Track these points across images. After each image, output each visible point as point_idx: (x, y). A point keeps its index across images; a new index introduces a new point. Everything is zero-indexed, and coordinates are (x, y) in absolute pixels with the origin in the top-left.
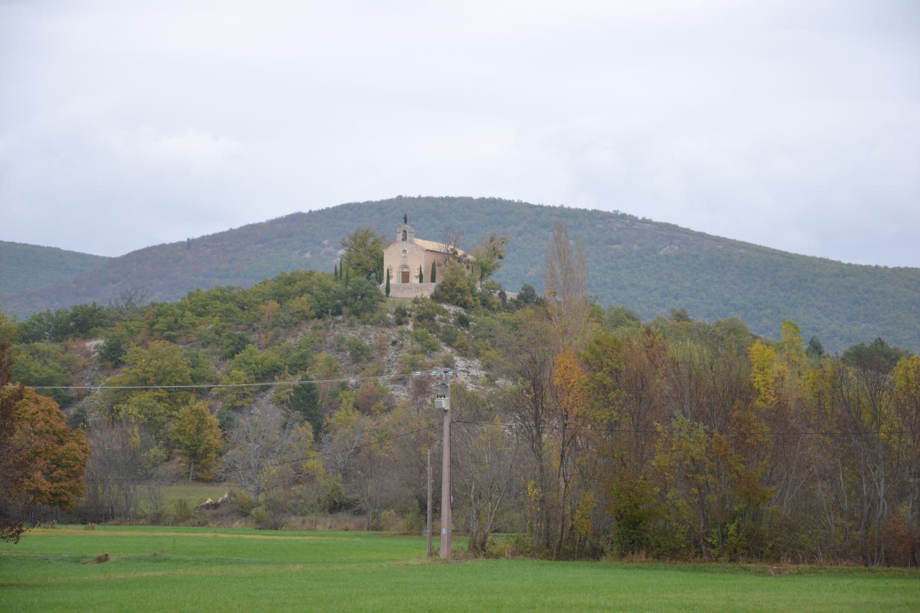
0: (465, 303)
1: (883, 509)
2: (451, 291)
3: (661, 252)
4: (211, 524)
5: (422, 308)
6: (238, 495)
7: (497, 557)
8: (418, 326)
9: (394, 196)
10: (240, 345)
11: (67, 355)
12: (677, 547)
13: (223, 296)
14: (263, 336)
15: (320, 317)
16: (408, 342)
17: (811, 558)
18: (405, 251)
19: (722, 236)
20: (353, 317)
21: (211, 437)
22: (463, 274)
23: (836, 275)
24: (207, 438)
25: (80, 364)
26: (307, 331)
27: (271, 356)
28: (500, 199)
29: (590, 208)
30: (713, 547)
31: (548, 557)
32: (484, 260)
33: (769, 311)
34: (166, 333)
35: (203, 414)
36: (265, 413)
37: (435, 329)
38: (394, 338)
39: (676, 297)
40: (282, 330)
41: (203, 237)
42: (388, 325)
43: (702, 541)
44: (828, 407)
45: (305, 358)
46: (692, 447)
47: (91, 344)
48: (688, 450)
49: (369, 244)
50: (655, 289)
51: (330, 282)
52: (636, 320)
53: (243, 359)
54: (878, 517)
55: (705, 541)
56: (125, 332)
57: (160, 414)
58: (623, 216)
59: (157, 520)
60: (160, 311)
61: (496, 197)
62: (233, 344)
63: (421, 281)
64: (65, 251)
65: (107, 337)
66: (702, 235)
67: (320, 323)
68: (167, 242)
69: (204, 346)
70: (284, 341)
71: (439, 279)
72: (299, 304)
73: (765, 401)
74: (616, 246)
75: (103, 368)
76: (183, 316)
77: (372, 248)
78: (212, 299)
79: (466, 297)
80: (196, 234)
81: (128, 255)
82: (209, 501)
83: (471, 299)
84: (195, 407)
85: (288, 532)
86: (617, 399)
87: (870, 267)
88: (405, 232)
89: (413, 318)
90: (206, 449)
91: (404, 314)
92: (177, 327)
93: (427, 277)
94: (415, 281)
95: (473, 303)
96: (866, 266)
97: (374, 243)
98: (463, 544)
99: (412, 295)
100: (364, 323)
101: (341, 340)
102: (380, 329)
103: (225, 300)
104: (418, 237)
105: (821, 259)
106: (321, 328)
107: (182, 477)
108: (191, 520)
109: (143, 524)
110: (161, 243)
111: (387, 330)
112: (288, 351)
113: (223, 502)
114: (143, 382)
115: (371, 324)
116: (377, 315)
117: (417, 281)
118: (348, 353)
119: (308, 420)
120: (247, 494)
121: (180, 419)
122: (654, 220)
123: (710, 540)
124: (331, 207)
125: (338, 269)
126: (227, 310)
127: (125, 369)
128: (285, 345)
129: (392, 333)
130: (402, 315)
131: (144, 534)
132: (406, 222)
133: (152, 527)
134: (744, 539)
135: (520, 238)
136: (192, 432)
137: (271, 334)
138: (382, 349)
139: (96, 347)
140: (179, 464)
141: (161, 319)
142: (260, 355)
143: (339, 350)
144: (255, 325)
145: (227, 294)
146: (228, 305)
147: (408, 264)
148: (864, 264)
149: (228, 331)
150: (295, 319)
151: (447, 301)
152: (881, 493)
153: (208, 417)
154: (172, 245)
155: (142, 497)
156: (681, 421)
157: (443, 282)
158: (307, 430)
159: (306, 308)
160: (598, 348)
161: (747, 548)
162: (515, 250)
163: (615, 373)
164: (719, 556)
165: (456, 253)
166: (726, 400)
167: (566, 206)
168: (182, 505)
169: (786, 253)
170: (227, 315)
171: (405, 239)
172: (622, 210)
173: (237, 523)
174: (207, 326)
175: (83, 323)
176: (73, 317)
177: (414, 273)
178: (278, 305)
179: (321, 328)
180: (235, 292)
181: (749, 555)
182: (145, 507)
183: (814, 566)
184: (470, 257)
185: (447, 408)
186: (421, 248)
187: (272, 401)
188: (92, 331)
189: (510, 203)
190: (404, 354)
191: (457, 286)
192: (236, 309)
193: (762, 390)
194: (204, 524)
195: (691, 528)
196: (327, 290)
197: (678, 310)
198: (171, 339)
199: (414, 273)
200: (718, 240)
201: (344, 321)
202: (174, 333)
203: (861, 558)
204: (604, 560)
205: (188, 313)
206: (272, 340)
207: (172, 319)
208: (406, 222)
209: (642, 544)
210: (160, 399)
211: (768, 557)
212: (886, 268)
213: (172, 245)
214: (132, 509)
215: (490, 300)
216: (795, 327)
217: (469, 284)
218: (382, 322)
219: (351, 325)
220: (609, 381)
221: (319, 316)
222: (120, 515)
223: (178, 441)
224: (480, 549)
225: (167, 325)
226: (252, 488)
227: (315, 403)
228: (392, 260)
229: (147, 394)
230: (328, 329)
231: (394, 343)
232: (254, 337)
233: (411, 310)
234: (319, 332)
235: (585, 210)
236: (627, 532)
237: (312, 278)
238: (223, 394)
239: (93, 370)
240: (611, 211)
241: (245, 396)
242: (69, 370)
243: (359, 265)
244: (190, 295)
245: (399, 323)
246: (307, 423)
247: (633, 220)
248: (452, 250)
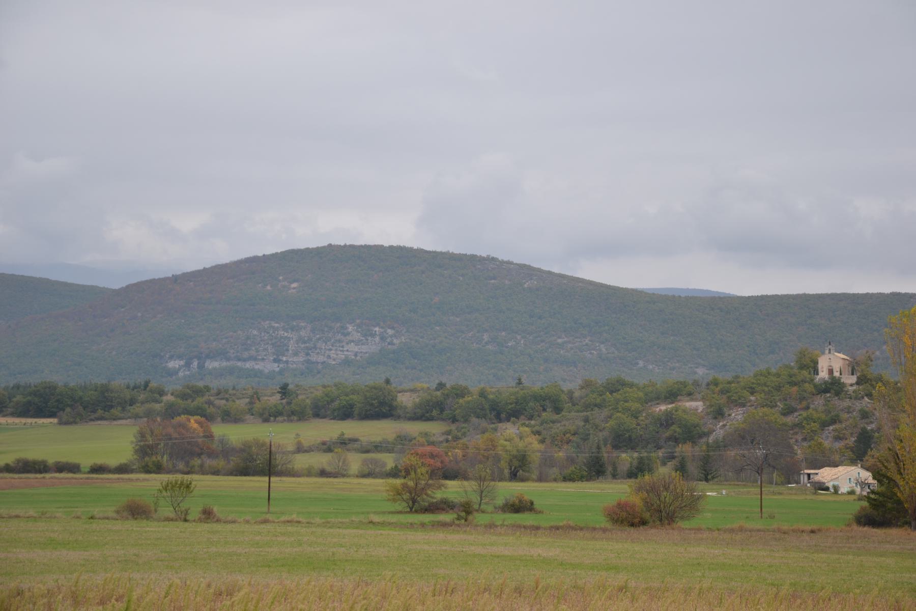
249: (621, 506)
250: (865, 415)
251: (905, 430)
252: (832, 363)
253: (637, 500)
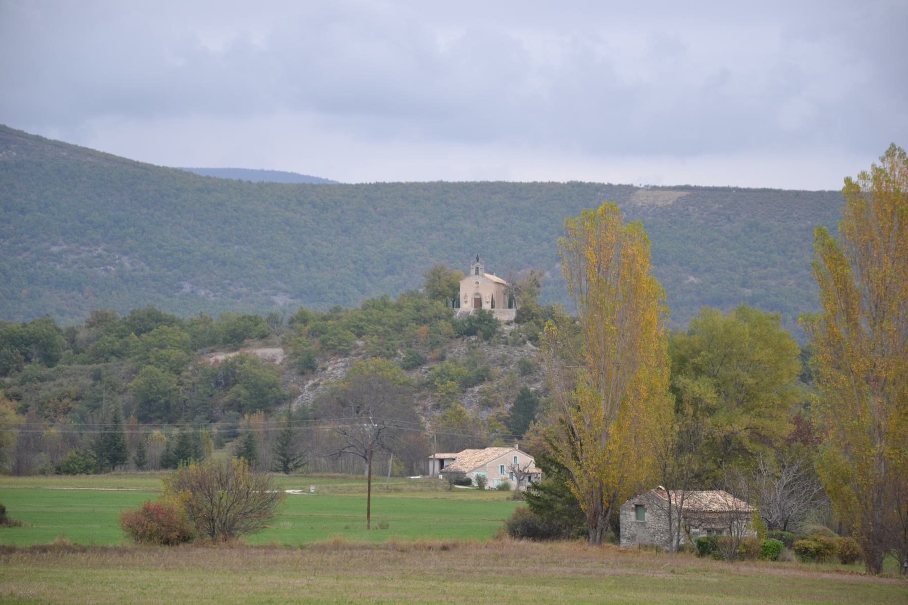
33: (132, 230)
171: (477, 273)
249: (150, 512)
250: (527, 369)
251: (584, 393)
252: (479, 289)
253: (175, 503)
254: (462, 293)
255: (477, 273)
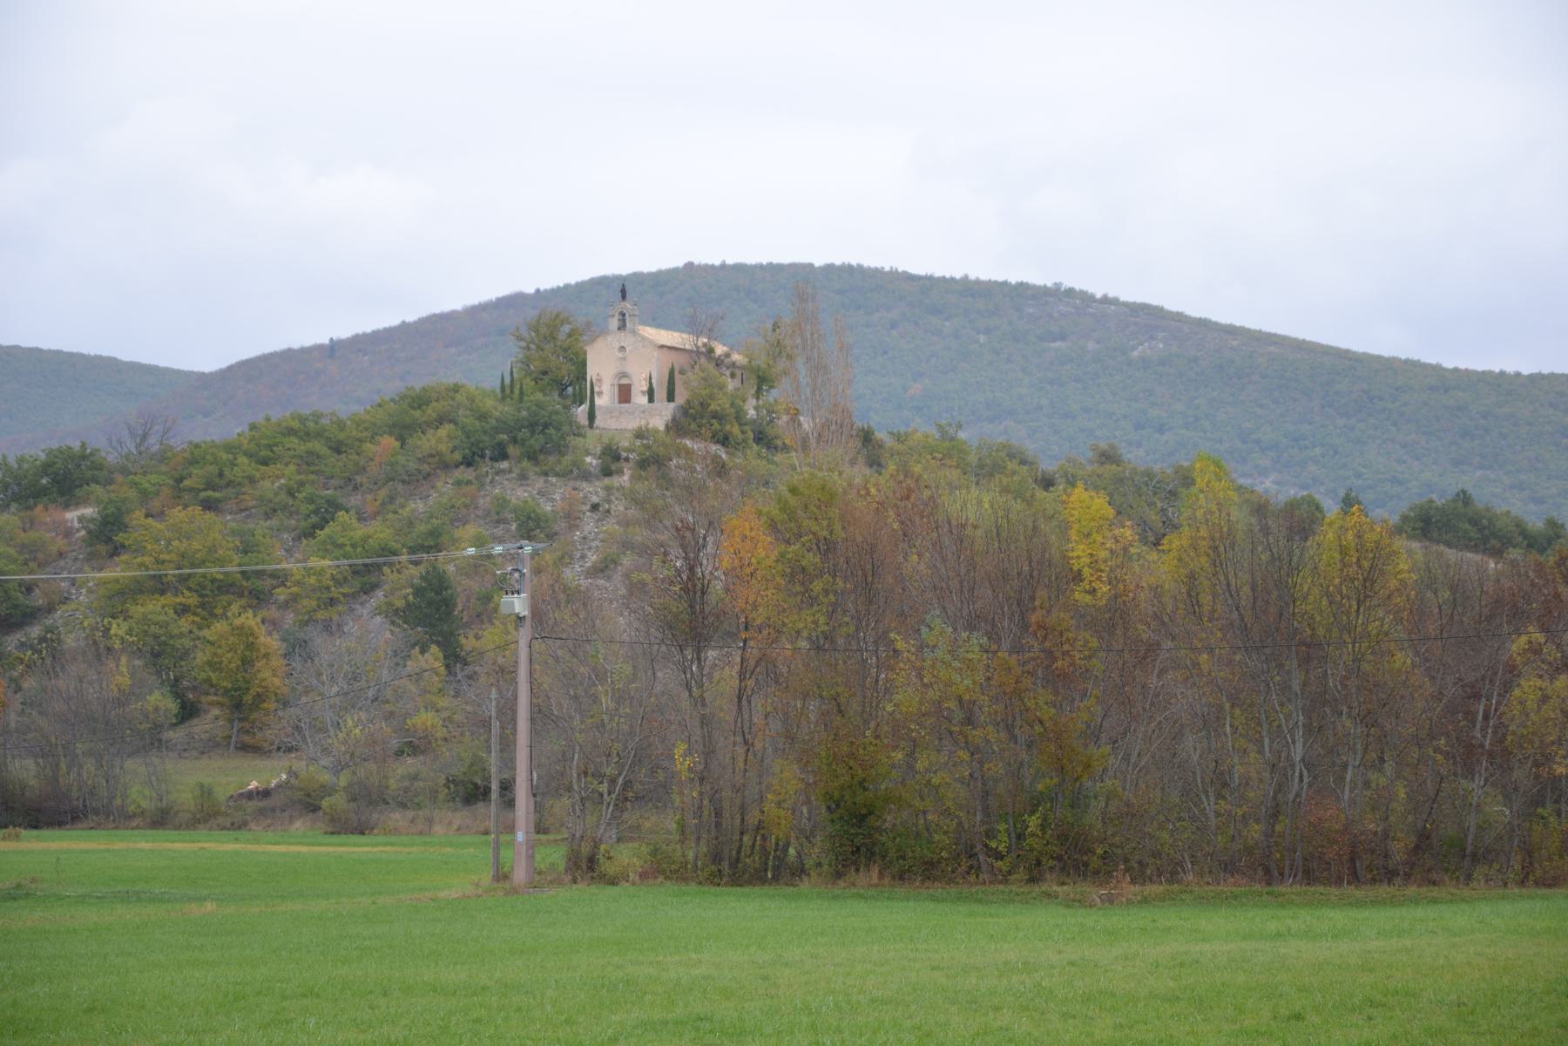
0: (726, 438)
1: (1301, 780)
2: (702, 417)
3: (1135, 354)
4: (252, 825)
5: (648, 447)
6: (303, 774)
7: (613, 882)
8: (640, 478)
9: (680, 263)
10: (326, 513)
11: (32, 535)
12: (936, 857)
13: (303, 429)
14: (369, 497)
15: (469, 465)
16: (619, 506)
17: (1171, 872)
18: (622, 348)
19: (1238, 324)
20: (525, 463)
21: (267, 674)
22: (722, 387)
23: (1433, 389)
24: (260, 675)
25: (54, 549)
26: (444, 489)
27: (379, 532)
28: (860, 267)
29: (1013, 280)
30: (999, 856)
31: (715, 879)
32: (761, 361)
33: (1318, 451)
34: (203, 495)
35: (252, 634)
36: (369, 630)
37: (666, 481)
38: (595, 499)
39: (1161, 429)
40: (400, 487)
41: (357, 336)
42: (586, 476)
43: (979, 847)
44: (1205, 599)
45: (440, 535)
46: (956, 678)
47: (72, 515)
48: (949, 684)
49: (562, 336)
50: (1125, 417)
51: (490, 403)
52: (1031, 464)
53: (330, 537)
54: (1291, 797)
55: (986, 846)
56: (132, 494)
57: (182, 635)
58: (1070, 292)
59: (161, 819)
60: (196, 455)
61: (854, 263)
62: (316, 512)
63: (651, 400)
64: (126, 363)
65: (99, 502)
66: (1204, 323)
67: (463, 473)
68: (296, 346)
69: (267, 516)
70: (403, 507)
71: (681, 397)
72: (433, 441)
73: (1093, 592)
74: (1057, 344)
75: (91, 557)
76: (233, 464)
77: (566, 345)
78: (284, 435)
79: (728, 427)
80: (344, 332)
81: (230, 368)
82: (253, 785)
83: (736, 430)
84: (238, 622)
85: (381, 839)
86: (826, 592)
87: (1491, 373)
88: (623, 315)
89: (631, 464)
90: (259, 695)
91: (617, 458)
92: (223, 482)
93: (661, 393)
94: (640, 399)
95: (740, 437)
96: (1483, 373)
97: (570, 336)
98: (554, 856)
99: (632, 424)
100: (546, 474)
101: (502, 503)
102: (571, 483)
103: (307, 435)
104: (644, 323)
105: (1407, 361)
106: (469, 483)
107: (218, 745)
108: (220, 820)
109: (137, 827)
110: (284, 346)
111: (584, 485)
112: (411, 524)
113: (278, 786)
114: (160, 586)
115: (557, 475)
116: (568, 459)
117: (645, 400)
118: (514, 527)
119: (438, 643)
120: (313, 768)
121: (212, 644)
122: (1123, 298)
123: (993, 844)
124: (573, 282)
125: (507, 381)
126: (310, 453)
127: (124, 557)
128: (405, 513)
129: (593, 491)
130: (612, 458)
131: (93, 846)
132: (624, 297)
133: (150, 832)
134: (1054, 845)
135: (894, 333)
136: (233, 666)
137: (383, 494)
138: (572, 519)
139: (80, 520)
140: (212, 721)
141: (195, 471)
142: (359, 531)
143: (498, 522)
144: (358, 479)
145: (311, 425)
146: (310, 445)
147: (628, 376)
148: (1480, 368)
149: (309, 489)
150: (426, 468)
151: (695, 435)
152: (1298, 752)
153: (262, 639)
154: (303, 350)
155: (137, 780)
156: (938, 630)
157: (688, 402)
158: (433, 658)
159: (443, 448)
160: (793, 501)
161: (1060, 858)
162: (885, 353)
163: (827, 547)
164: (1010, 872)
165: (711, 351)
166: (1020, 591)
167: (972, 277)
168: (205, 792)
169: (1347, 351)
170: (309, 461)
171: (622, 326)
172: (1068, 282)
173: (298, 824)
174: (272, 484)
175: (63, 478)
176: (46, 468)
177: (639, 386)
178: (397, 444)
179: (469, 483)
180: (325, 421)
181: (1063, 869)
182: (139, 795)
183: (1176, 887)
184: (736, 357)
185: (525, 613)
186: (651, 342)
187: (378, 611)
188: (78, 492)
189: (877, 273)
190: (611, 526)
191: (712, 407)
192: (324, 450)
193: (1086, 572)
194: (241, 826)
195: (960, 824)
196: (483, 417)
197: (1103, 445)
198: (208, 505)
199: (639, 386)
200: (1232, 331)
201: (510, 471)
202: (217, 495)
203: (1260, 872)
204: (804, 886)
205: (242, 460)
206: (383, 504)
207: (213, 469)
208: (624, 297)
209: (873, 854)
210: (183, 610)
211: (1096, 873)
212: (1518, 375)
213: (304, 351)
214: (118, 802)
215: (770, 432)
216: (1217, 464)
217: (732, 405)
218: (576, 472)
219: (523, 477)
220: (811, 559)
221: (468, 463)
222: (97, 814)
223: (208, 681)
224: (587, 866)
225: (207, 481)
226: (326, 761)
227: (449, 613)
228: (601, 365)
229: (163, 601)
230: (482, 485)
231: (595, 507)
232: (355, 500)
233: (628, 450)
234: (465, 489)
235: (1005, 284)
236: (846, 832)
237: (458, 397)
238: (295, 598)
239: (76, 559)
240: (1049, 284)
241: (332, 602)
242: (35, 559)
243: (545, 373)
244: (253, 427)
245: (607, 472)
246: (434, 648)
247: (1087, 298)
248: (705, 345)
254: (591, 372)
255: (622, 326)
